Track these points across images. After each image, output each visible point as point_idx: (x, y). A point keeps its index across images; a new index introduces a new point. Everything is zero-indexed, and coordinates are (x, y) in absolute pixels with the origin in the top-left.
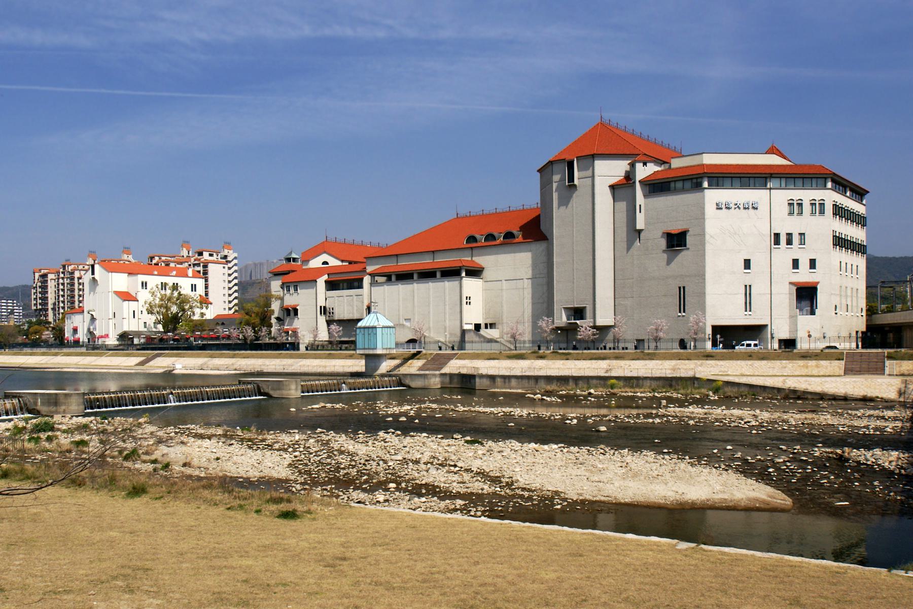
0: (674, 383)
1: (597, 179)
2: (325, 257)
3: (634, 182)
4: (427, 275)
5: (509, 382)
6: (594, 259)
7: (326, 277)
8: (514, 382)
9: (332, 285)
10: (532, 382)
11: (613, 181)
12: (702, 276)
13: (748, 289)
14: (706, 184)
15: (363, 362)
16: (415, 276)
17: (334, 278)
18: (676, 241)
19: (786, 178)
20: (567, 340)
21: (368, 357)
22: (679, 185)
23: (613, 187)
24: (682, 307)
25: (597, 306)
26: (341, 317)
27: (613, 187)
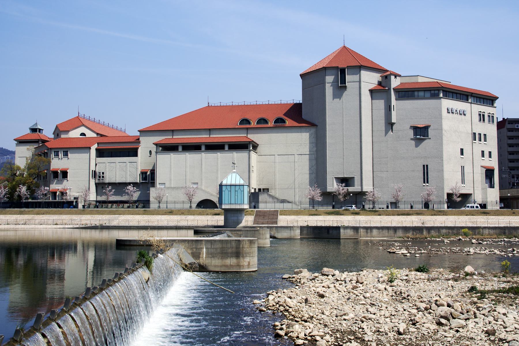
0: (507, 231)
1: (362, 84)
2: (83, 130)
3: (389, 89)
4: (194, 148)
5: (371, 232)
6: (361, 142)
7: (96, 146)
8: (375, 232)
9: (100, 153)
10: (391, 232)
11: (372, 87)
12: (441, 157)
13: (463, 168)
14: (441, 95)
15: (222, 218)
16: (203, 148)
17: (103, 147)
18: (421, 133)
19: (476, 97)
20: (332, 201)
21: (227, 212)
22: (421, 94)
23: (371, 91)
24: (426, 180)
25: (363, 177)
26: (113, 181)
27: (371, 91)
